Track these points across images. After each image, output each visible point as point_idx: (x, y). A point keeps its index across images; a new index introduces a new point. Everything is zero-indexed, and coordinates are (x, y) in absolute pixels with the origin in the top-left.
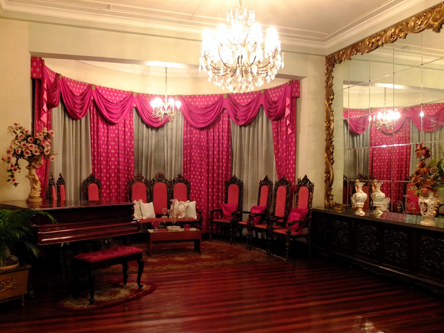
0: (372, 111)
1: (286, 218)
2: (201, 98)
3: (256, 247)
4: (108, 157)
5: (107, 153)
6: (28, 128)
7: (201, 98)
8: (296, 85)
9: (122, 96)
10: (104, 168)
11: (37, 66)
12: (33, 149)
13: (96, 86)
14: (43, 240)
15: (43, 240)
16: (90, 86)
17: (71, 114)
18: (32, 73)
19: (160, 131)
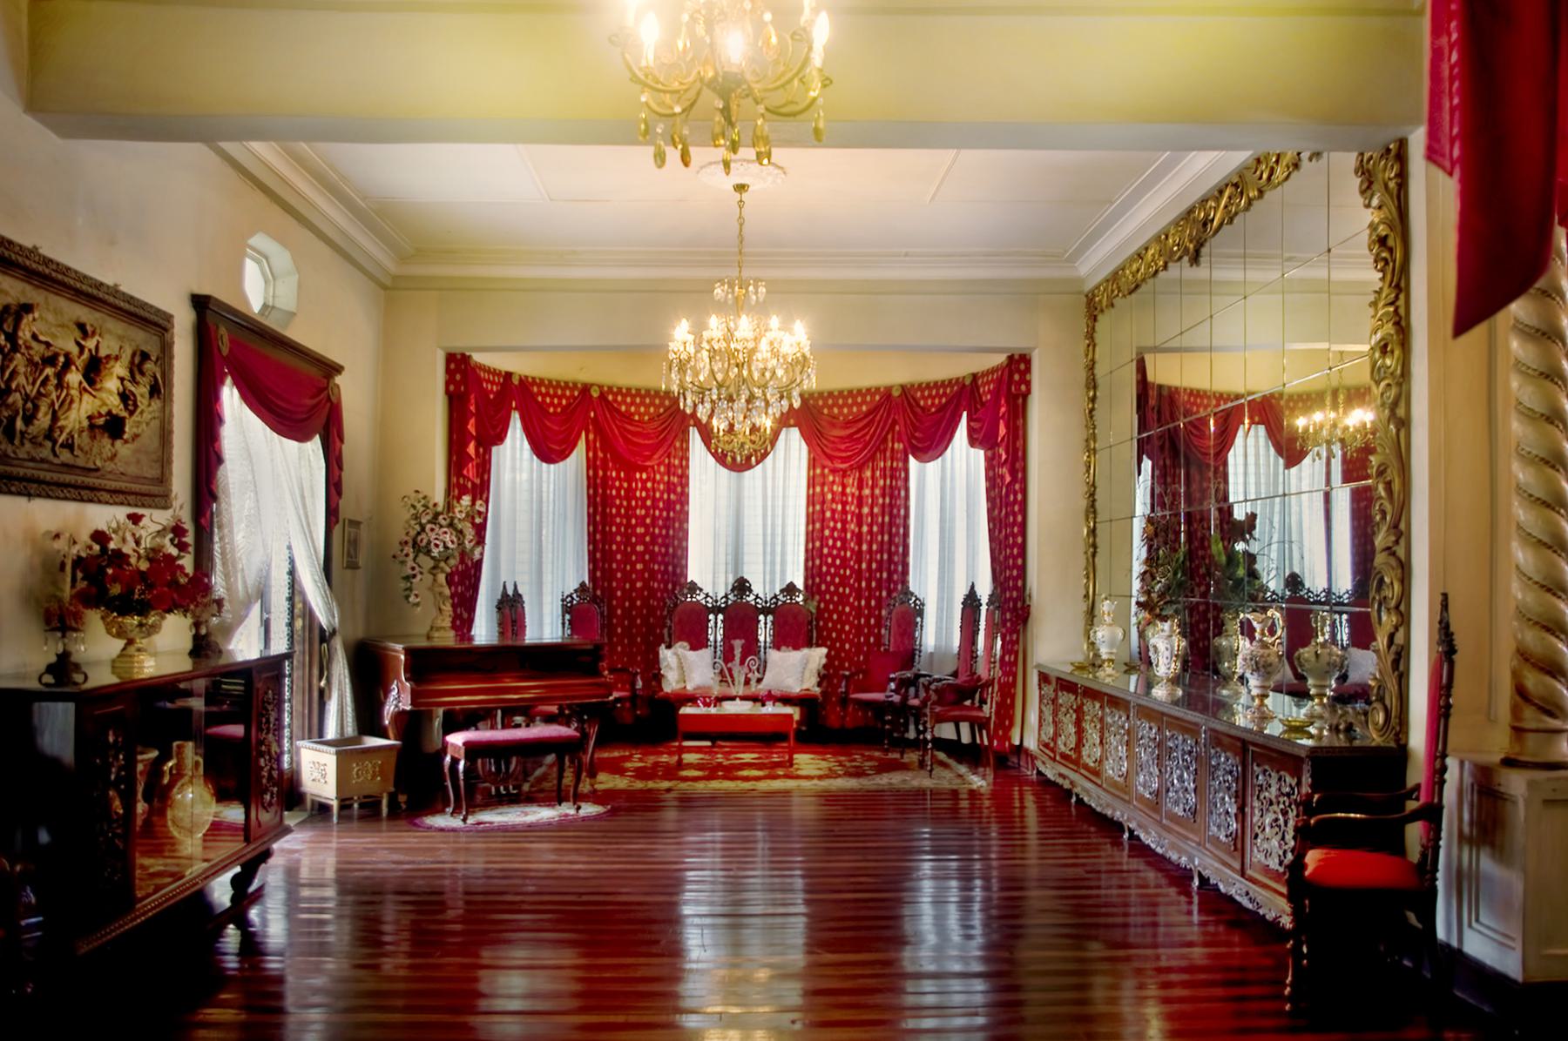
0: (1561, 258)
1: (1329, 592)
2: (845, 398)
3: (960, 762)
4: (627, 543)
5: (627, 536)
6: (439, 496)
7: (845, 398)
8: (1022, 366)
9: (662, 404)
10: (618, 570)
11: (457, 370)
12: (447, 538)
13: (601, 387)
14: (23, 923)
15: (23, 923)
16: (586, 389)
17: (548, 449)
18: (447, 384)
19: (753, 476)
